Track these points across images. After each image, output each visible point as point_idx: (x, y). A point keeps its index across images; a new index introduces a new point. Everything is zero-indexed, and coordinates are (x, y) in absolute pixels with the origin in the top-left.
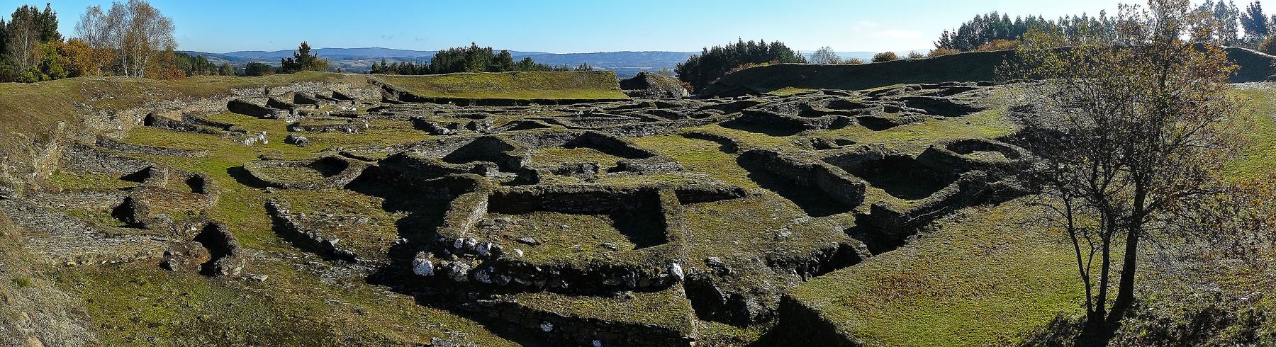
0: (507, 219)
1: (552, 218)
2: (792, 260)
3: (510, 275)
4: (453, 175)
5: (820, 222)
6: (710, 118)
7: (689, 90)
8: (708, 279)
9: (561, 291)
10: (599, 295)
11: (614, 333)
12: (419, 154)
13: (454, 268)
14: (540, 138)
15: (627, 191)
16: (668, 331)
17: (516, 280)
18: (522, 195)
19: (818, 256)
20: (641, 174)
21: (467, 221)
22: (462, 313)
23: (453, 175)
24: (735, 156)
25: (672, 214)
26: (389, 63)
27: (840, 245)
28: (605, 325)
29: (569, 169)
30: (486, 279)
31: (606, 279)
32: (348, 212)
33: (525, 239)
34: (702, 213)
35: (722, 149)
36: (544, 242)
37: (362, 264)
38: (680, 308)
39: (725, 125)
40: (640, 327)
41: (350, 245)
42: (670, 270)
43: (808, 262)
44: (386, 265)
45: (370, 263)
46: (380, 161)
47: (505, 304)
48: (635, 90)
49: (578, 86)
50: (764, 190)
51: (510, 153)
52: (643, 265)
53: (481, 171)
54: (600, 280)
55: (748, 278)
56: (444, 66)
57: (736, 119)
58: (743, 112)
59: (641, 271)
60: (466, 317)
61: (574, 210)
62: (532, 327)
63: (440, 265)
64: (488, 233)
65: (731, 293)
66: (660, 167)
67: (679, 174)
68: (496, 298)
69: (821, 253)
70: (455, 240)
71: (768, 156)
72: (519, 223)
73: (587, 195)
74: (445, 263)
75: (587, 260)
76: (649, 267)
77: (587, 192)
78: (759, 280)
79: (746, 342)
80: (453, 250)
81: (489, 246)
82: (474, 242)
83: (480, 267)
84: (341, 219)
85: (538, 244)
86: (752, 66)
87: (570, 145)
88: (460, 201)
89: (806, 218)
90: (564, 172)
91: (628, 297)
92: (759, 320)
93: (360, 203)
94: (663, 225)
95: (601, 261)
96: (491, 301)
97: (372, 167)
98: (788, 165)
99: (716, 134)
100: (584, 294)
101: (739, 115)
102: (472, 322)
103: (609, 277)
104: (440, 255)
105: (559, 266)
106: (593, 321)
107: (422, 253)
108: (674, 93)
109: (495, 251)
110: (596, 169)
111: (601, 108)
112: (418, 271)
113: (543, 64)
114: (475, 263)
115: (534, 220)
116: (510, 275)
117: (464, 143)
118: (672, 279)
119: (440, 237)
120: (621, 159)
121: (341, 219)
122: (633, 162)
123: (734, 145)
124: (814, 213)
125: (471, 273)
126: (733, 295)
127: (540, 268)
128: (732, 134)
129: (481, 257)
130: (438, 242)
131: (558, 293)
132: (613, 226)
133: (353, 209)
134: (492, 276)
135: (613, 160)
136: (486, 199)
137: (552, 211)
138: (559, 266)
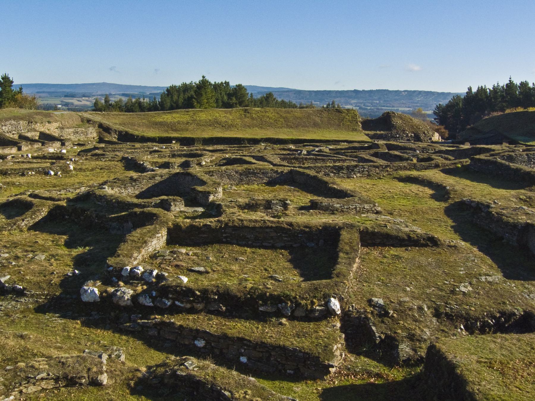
0: (183, 250)
1: (227, 250)
2: (462, 315)
3: (171, 298)
4: (137, 210)
5: (513, 285)
6: (432, 162)
7: (442, 135)
8: (367, 318)
9: (218, 313)
10: (253, 319)
11: (259, 352)
12: (108, 191)
13: (119, 293)
14: (241, 174)
15: (310, 228)
16: (309, 356)
17: (177, 303)
18: (201, 228)
19: (493, 317)
20: (333, 214)
21: (140, 253)
22: (122, 331)
23: (137, 210)
24: (444, 205)
25: (347, 254)
26: (113, 100)
27: (524, 311)
28: (251, 344)
29: (256, 204)
30: (147, 302)
31: (262, 305)
32: (27, 251)
33: (197, 269)
34: (385, 257)
35: (433, 197)
36: (214, 271)
37: (32, 296)
38: (327, 338)
39: (448, 172)
40: (284, 349)
41: (22, 280)
42: (327, 303)
43: (480, 321)
44: (56, 295)
45: (40, 295)
46: (69, 200)
47: (163, 323)
48: (378, 132)
49: (316, 125)
50: (463, 243)
51: (200, 188)
52: (300, 296)
53: (165, 206)
54: (256, 306)
55: (409, 324)
56: (175, 103)
57: (463, 166)
58: (472, 159)
59: (297, 301)
60: (126, 335)
61: (254, 244)
62: (187, 343)
63: (106, 291)
64: (161, 263)
65: (386, 334)
66: (356, 208)
67: (374, 216)
68: (155, 318)
69: (498, 315)
70: (122, 269)
71: (480, 209)
72: (195, 254)
73: (268, 230)
74: (111, 290)
75: (246, 287)
76: (306, 299)
77: (268, 227)
78: (419, 328)
79: (388, 380)
80: (120, 277)
81: (155, 273)
82: (140, 270)
83: (144, 292)
84: (17, 258)
85: (207, 272)
86: (520, 109)
87: (271, 183)
88: (137, 234)
89: (497, 277)
90: (251, 207)
91: (281, 324)
92: (407, 363)
93: (40, 242)
94: (334, 260)
95: (260, 289)
96: (150, 321)
97: (59, 207)
98: (498, 220)
99: (433, 180)
100: (240, 317)
101: (467, 162)
102: (132, 339)
103: (265, 304)
104: (107, 282)
105: (218, 291)
106: (241, 340)
107: (90, 282)
108: (422, 136)
109: (160, 277)
110: (285, 206)
111: (326, 149)
112: (85, 298)
113: (286, 100)
114: (139, 289)
115: (211, 253)
116: (171, 298)
117: (158, 179)
118: (329, 313)
119: (109, 266)
120: (315, 198)
121: (17, 258)
122: (325, 201)
123: (448, 193)
124: (508, 276)
125: (134, 298)
126: (387, 336)
127: (199, 292)
128: (449, 181)
129: (146, 283)
130: (107, 271)
131: (215, 315)
132: (290, 261)
133: (34, 248)
134: (153, 299)
135: (306, 198)
136: (164, 232)
137: (232, 244)
138: (218, 291)
